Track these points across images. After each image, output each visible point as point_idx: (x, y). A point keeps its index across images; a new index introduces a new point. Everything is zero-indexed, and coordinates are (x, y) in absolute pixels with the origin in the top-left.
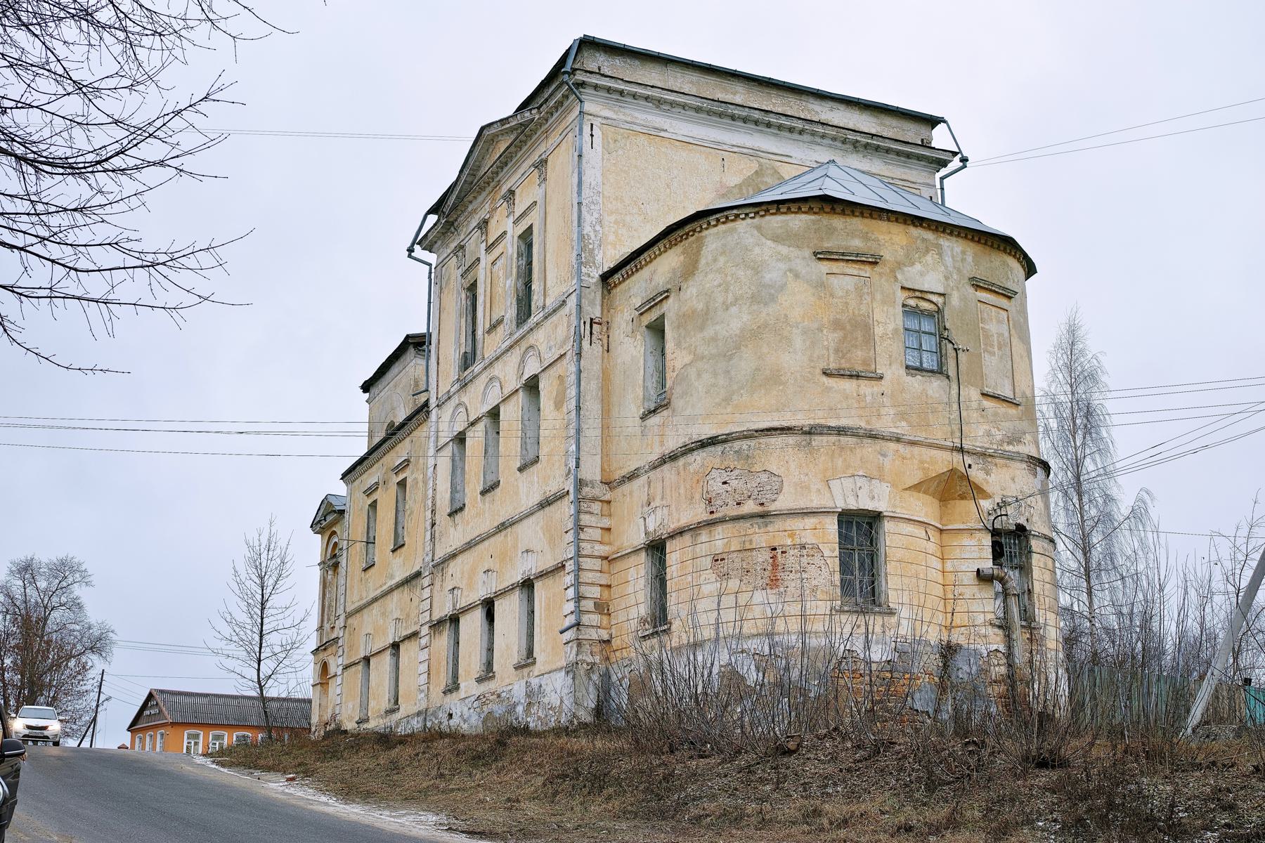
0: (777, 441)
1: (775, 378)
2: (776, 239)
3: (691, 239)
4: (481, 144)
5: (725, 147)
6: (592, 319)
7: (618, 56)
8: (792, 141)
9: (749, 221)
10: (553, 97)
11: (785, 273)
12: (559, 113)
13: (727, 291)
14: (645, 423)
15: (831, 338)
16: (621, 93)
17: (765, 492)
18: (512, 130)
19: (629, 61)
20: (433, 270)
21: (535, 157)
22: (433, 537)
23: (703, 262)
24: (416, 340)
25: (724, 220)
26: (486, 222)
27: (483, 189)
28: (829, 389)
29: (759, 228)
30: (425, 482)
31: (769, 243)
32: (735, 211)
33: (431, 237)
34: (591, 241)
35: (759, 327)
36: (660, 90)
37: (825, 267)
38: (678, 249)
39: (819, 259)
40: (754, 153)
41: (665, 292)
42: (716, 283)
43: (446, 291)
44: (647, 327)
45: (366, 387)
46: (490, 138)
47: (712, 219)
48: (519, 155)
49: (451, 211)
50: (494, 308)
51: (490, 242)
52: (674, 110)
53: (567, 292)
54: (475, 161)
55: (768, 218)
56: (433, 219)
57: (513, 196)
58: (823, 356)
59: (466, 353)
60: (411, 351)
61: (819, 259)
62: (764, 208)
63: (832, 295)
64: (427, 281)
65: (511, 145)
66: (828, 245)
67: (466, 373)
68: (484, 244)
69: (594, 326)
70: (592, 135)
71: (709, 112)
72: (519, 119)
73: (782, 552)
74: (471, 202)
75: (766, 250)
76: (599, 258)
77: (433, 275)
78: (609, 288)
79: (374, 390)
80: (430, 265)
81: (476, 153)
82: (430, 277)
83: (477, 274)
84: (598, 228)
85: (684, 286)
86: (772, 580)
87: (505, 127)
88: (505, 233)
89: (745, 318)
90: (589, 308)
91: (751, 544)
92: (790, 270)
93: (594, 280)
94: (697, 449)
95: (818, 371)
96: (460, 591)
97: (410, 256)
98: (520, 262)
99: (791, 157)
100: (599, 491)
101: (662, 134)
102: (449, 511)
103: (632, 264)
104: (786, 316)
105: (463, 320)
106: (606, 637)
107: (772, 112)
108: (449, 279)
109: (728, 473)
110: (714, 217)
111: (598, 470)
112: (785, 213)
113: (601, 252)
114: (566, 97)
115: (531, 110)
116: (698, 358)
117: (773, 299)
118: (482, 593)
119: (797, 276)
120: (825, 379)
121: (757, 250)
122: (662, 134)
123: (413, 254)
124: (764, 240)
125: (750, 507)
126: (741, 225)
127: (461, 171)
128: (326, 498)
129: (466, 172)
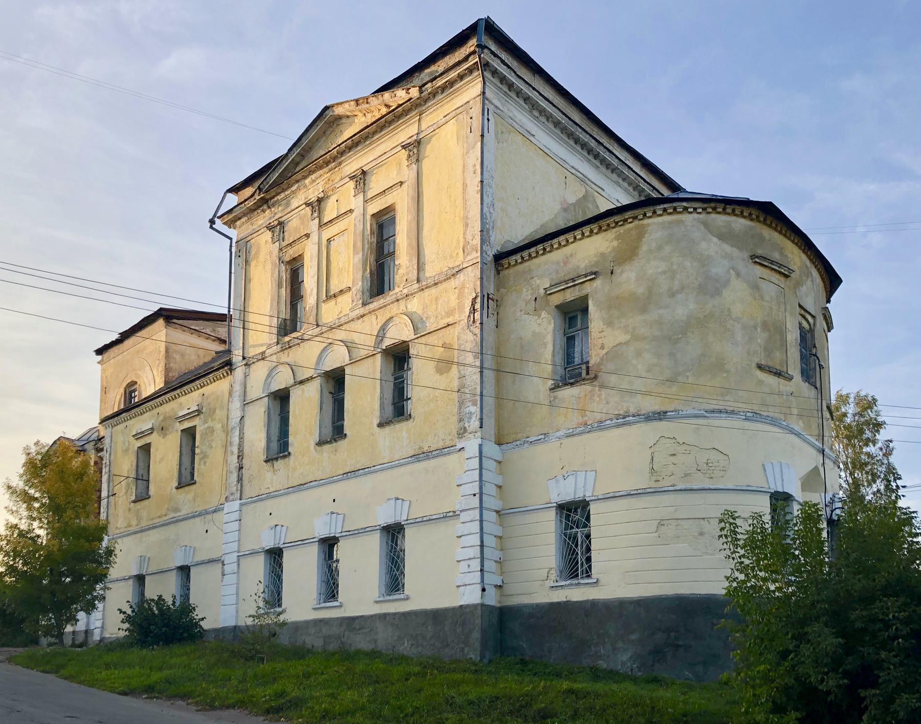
1: (719, 366)
2: (721, 237)
3: (628, 226)
4: (320, 124)
5: (568, 167)
6: (488, 294)
7: (504, 51)
8: (604, 177)
9: (695, 216)
11: (729, 270)
12: (444, 94)
13: (673, 278)
14: (555, 394)
15: (761, 337)
16: (511, 86)
17: (713, 468)
19: (510, 59)
20: (234, 244)
22: (240, 479)
23: (644, 248)
24: (168, 313)
25: (672, 211)
27: (321, 168)
28: (760, 382)
29: (705, 224)
30: (227, 432)
31: (715, 239)
32: (685, 204)
34: (487, 221)
36: (537, 94)
37: (759, 270)
38: (611, 234)
39: (756, 262)
40: (583, 180)
41: (592, 273)
42: (660, 270)
43: (253, 264)
44: (557, 307)
45: (99, 352)
46: (331, 119)
47: (659, 209)
48: (375, 138)
52: (540, 118)
53: (458, 266)
55: (713, 216)
57: (364, 177)
58: (758, 351)
60: (161, 322)
61: (756, 262)
62: (713, 205)
63: (762, 298)
64: (229, 253)
66: (760, 252)
69: (490, 301)
71: (564, 130)
75: (712, 247)
78: (500, 268)
79: (106, 355)
80: (231, 239)
81: (312, 133)
82: (230, 250)
84: (492, 211)
85: (617, 270)
88: (351, 211)
89: (692, 306)
92: (733, 268)
95: (754, 365)
97: (211, 227)
98: (373, 240)
99: (603, 190)
101: (531, 138)
103: (540, 247)
104: (729, 309)
105: (283, 291)
106: (499, 583)
110: (662, 206)
112: (729, 214)
116: (636, 338)
117: (717, 292)
119: (738, 275)
121: (704, 245)
122: (531, 138)
123: (214, 226)
124: (710, 236)
126: (689, 219)
127: (290, 150)
128: (59, 439)
129: (297, 151)
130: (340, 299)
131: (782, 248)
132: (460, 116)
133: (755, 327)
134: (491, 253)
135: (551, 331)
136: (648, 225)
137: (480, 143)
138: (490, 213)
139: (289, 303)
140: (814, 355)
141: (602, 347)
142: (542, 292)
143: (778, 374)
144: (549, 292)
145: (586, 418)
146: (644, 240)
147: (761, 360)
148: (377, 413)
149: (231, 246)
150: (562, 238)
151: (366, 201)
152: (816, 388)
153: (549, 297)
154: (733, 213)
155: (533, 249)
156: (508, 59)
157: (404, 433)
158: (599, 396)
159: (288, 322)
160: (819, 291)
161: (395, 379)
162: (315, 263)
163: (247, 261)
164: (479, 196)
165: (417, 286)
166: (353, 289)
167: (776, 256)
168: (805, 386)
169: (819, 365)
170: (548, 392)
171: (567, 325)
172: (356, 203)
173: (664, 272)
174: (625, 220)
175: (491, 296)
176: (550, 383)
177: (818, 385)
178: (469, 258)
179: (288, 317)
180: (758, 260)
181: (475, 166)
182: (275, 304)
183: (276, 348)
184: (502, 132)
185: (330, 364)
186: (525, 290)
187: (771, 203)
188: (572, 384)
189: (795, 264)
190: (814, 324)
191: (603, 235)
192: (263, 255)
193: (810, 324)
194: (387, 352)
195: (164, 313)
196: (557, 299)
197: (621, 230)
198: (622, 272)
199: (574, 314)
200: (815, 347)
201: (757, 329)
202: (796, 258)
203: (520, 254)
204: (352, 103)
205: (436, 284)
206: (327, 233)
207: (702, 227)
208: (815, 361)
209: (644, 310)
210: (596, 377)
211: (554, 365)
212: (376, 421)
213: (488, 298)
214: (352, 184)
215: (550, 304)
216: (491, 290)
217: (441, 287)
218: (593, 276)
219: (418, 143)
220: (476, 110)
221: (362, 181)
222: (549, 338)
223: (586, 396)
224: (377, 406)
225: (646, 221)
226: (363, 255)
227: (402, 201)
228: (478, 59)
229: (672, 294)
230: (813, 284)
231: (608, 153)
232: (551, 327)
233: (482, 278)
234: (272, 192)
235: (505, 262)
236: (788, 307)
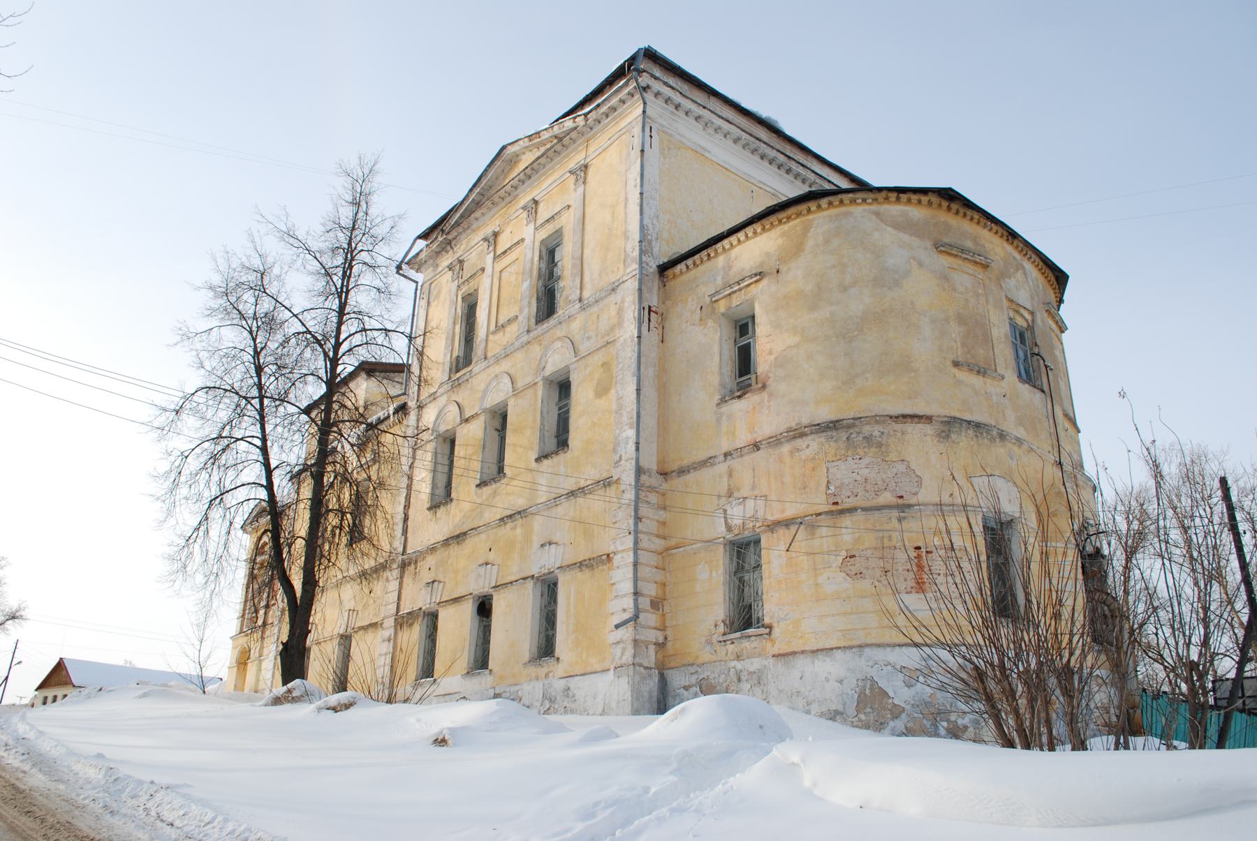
0: (913, 429)
2: (897, 226)
3: (792, 223)
4: (498, 163)
5: (754, 182)
6: (650, 307)
10: (606, 102)
12: (609, 119)
15: (955, 331)
18: (543, 144)
20: (419, 287)
21: (488, 230)
24: (372, 367)
26: (496, 235)
28: (959, 383)
29: (877, 214)
31: (889, 229)
33: (423, 256)
34: (649, 232)
35: (883, 311)
37: (946, 261)
39: (941, 252)
41: (756, 275)
43: (433, 304)
47: (824, 202)
49: (453, 227)
50: (500, 311)
51: (499, 252)
53: (618, 280)
54: (488, 180)
56: (422, 244)
59: (458, 356)
60: (363, 375)
63: (954, 290)
65: (542, 155)
67: (458, 375)
68: (492, 254)
69: (652, 313)
70: (651, 136)
72: (556, 130)
73: (927, 552)
74: (477, 219)
75: (887, 237)
76: (656, 250)
77: (418, 292)
78: (665, 280)
80: (417, 282)
82: (416, 293)
83: (478, 283)
84: (655, 222)
86: (918, 583)
87: (533, 142)
88: (523, 240)
90: (647, 295)
91: (890, 541)
92: (914, 258)
93: (652, 270)
94: (812, 433)
95: (949, 363)
96: (441, 585)
97: (398, 272)
100: (654, 480)
102: (429, 505)
104: (912, 303)
106: (661, 640)
107: (793, 159)
108: (439, 292)
109: (856, 461)
111: (655, 460)
113: (658, 245)
114: (631, 95)
115: (575, 118)
117: (897, 284)
118: (479, 586)
119: (920, 264)
120: (955, 370)
121: (876, 235)
124: (883, 225)
125: (887, 498)
127: (471, 190)
129: (477, 190)
130: (508, 329)
131: (976, 237)
132: (624, 137)
133: (947, 320)
134: (653, 266)
135: (718, 340)
136: (813, 220)
137: (639, 159)
138: (653, 224)
139: (463, 339)
140: (1038, 355)
141: (770, 353)
142: (708, 300)
143: (981, 372)
144: (714, 299)
145: (755, 435)
146: (809, 234)
147: (957, 357)
148: (536, 448)
149: (416, 289)
150: (726, 243)
151: (536, 229)
152: (1043, 391)
153: (715, 305)
154: (909, 201)
155: (697, 257)
156: (677, 84)
157: (562, 467)
158: (769, 407)
159: (461, 360)
160: (1038, 286)
161: (560, 409)
162: (487, 296)
163: (429, 303)
164: (638, 208)
165: (579, 305)
166: (520, 318)
167: (969, 244)
168: (1025, 389)
169: (1045, 366)
170: (715, 408)
171: (738, 334)
172: (528, 232)
173: (834, 266)
174: (789, 218)
175: (653, 309)
176: (717, 397)
177: (1046, 388)
178: (629, 270)
179: (462, 354)
180: (942, 248)
181: (636, 180)
182: (450, 342)
183: (446, 387)
184: (669, 149)
185: (493, 400)
186: (690, 299)
187: (950, 189)
188: (739, 397)
189: (996, 254)
190: (1033, 321)
191: (765, 235)
192: (444, 292)
193: (1027, 321)
194: (549, 382)
195: (367, 367)
196: (722, 307)
197: (786, 227)
198: (789, 270)
199: (744, 322)
200: (1036, 345)
201: (949, 323)
202: (997, 248)
203: (685, 262)
204: (526, 139)
205: (597, 301)
206: (499, 266)
207: (874, 217)
208: (1038, 360)
209: (813, 307)
210: (764, 387)
211: (721, 374)
212: (535, 456)
213: (650, 311)
214: (525, 215)
215: (717, 311)
216: (654, 301)
217: (601, 304)
218: (758, 277)
219: (586, 166)
220: (637, 130)
221: (533, 211)
222: (716, 348)
223: (754, 408)
224: (537, 441)
225: (811, 217)
226: (531, 282)
227: (568, 221)
228: (635, 84)
229: (844, 289)
230: (1026, 278)
231: (801, 168)
232: (717, 337)
233: (640, 290)
234: (454, 233)
235: (670, 272)
236: (991, 300)
